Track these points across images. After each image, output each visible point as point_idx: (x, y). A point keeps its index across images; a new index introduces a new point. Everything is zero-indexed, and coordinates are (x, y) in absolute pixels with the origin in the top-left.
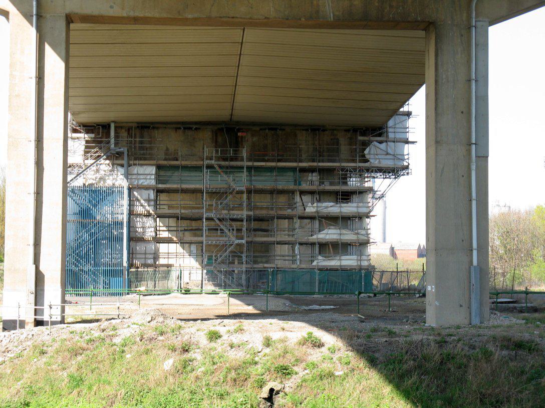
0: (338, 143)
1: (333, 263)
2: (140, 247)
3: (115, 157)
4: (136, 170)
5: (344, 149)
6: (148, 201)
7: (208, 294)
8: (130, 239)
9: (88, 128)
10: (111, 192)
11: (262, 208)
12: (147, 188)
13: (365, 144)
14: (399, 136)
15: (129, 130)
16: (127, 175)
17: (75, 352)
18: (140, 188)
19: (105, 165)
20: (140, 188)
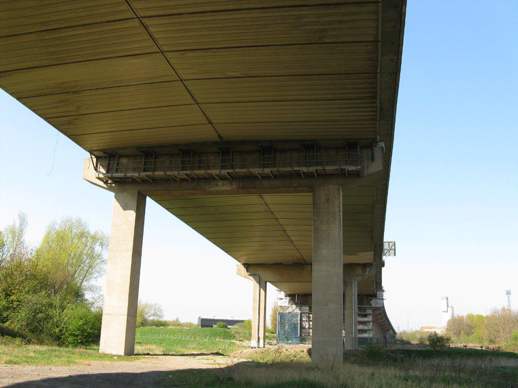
0: (363, 299)
1: (361, 336)
2: (304, 331)
3: (296, 304)
4: (302, 308)
5: (365, 302)
6: (307, 317)
7: (88, 181)
8: (301, 328)
9: (289, 295)
10: (296, 314)
11: (223, 178)
12: (306, 313)
13: (371, 300)
14: (381, 297)
15: (301, 296)
16: (300, 309)
17: (262, 353)
18: (304, 313)
19: (294, 306)
20: (304, 313)
